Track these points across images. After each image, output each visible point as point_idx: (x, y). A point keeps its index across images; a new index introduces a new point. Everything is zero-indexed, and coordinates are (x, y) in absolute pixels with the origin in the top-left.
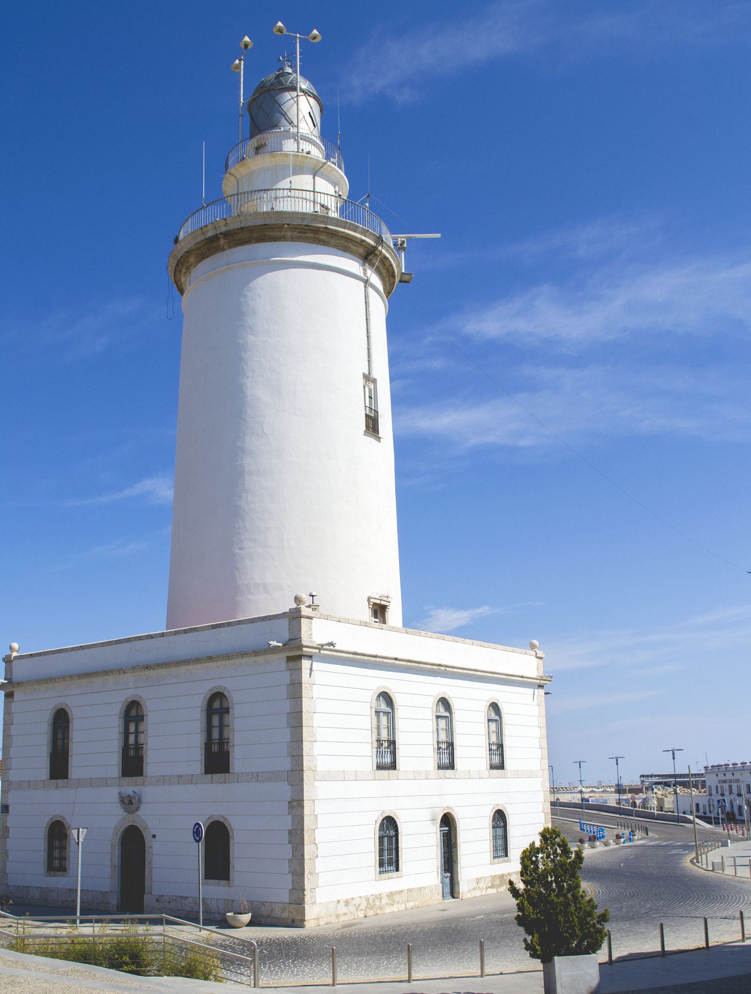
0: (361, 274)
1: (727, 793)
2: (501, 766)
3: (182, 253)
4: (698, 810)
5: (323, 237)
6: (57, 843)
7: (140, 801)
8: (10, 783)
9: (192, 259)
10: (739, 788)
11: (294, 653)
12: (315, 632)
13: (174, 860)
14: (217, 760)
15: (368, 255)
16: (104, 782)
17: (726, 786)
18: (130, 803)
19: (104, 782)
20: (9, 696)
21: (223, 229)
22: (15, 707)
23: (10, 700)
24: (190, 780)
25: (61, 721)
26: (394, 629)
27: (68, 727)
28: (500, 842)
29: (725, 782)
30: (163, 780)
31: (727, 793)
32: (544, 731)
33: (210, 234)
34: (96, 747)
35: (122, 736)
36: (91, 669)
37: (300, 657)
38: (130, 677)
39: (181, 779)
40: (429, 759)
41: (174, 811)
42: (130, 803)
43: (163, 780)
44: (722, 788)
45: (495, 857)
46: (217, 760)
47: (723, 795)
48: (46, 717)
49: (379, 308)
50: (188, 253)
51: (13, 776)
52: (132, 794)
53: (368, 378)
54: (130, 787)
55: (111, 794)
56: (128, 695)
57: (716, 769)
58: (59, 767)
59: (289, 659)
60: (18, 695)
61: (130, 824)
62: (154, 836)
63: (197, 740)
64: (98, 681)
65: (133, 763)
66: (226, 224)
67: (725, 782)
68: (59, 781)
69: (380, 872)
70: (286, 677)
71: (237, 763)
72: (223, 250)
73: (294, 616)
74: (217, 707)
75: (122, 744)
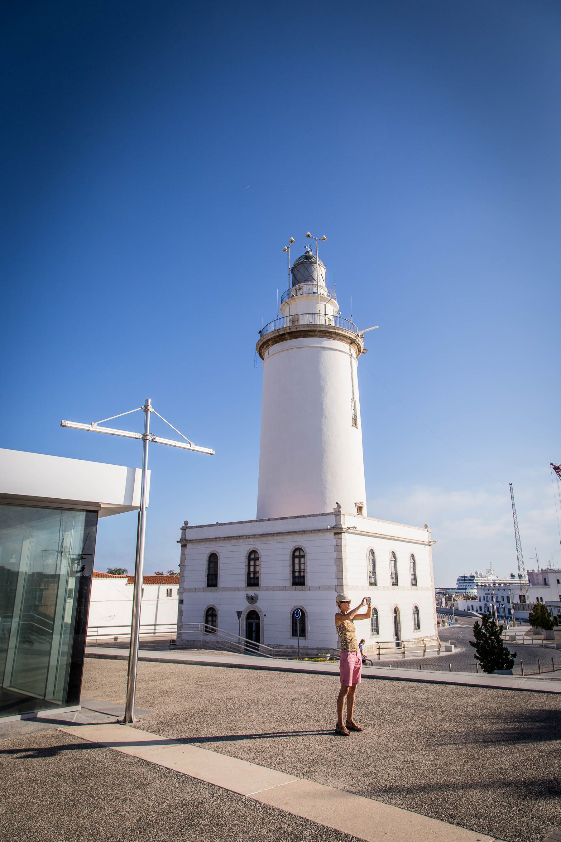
0: (348, 352)
1: (490, 600)
2: (375, 584)
3: (266, 340)
4: (481, 610)
5: (333, 336)
6: (210, 619)
7: (257, 599)
8: (184, 589)
9: (270, 343)
10: (497, 598)
11: (337, 531)
12: (347, 522)
13: (276, 627)
14: (298, 580)
15: (352, 342)
16: (238, 589)
17: (489, 596)
18: (252, 599)
19: (238, 589)
20: (184, 546)
21: (288, 331)
22: (187, 551)
23: (184, 548)
24: (284, 588)
25: (213, 559)
26: (364, 518)
27: (217, 562)
28: (374, 627)
29: (489, 594)
30: (269, 589)
31: (490, 600)
32: (432, 568)
33: (282, 333)
34: (233, 570)
35: (247, 567)
36: (231, 535)
37: (341, 533)
38: (252, 540)
39: (279, 588)
40: (389, 582)
41: (277, 605)
42: (252, 599)
43: (269, 589)
44: (487, 597)
45: (372, 635)
46: (298, 580)
47: (487, 601)
48: (206, 557)
49: (355, 363)
50: (269, 340)
51: (186, 585)
52: (254, 595)
53: (353, 399)
54: (252, 592)
55: (242, 595)
56: (251, 547)
57: (483, 587)
58: (212, 581)
59: (335, 534)
60: (189, 546)
61: (252, 609)
62: (265, 615)
63: (288, 570)
64: (234, 541)
65: (253, 581)
66: (290, 329)
67: (489, 594)
68: (212, 588)
69: (372, 635)
70: (334, 542)
71: (309, 581)
72: (287, 340)
73: (337, 513)
74: (298, 554)
75: (247, 571)
